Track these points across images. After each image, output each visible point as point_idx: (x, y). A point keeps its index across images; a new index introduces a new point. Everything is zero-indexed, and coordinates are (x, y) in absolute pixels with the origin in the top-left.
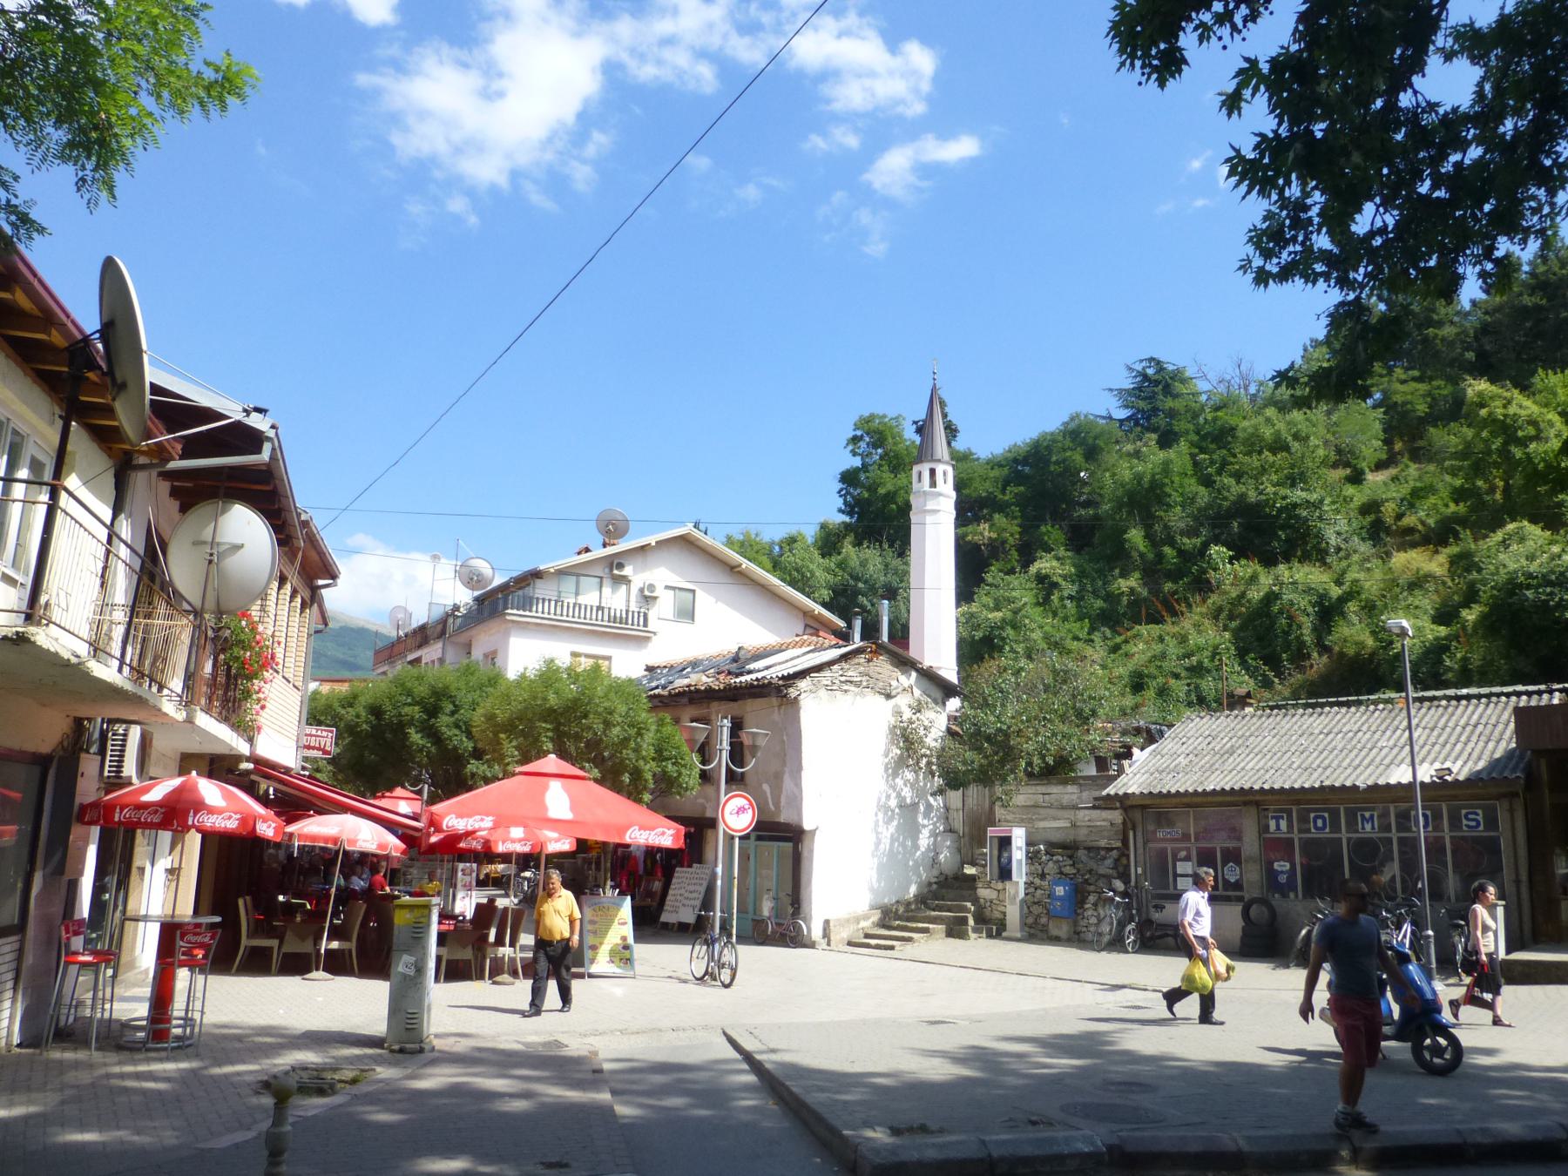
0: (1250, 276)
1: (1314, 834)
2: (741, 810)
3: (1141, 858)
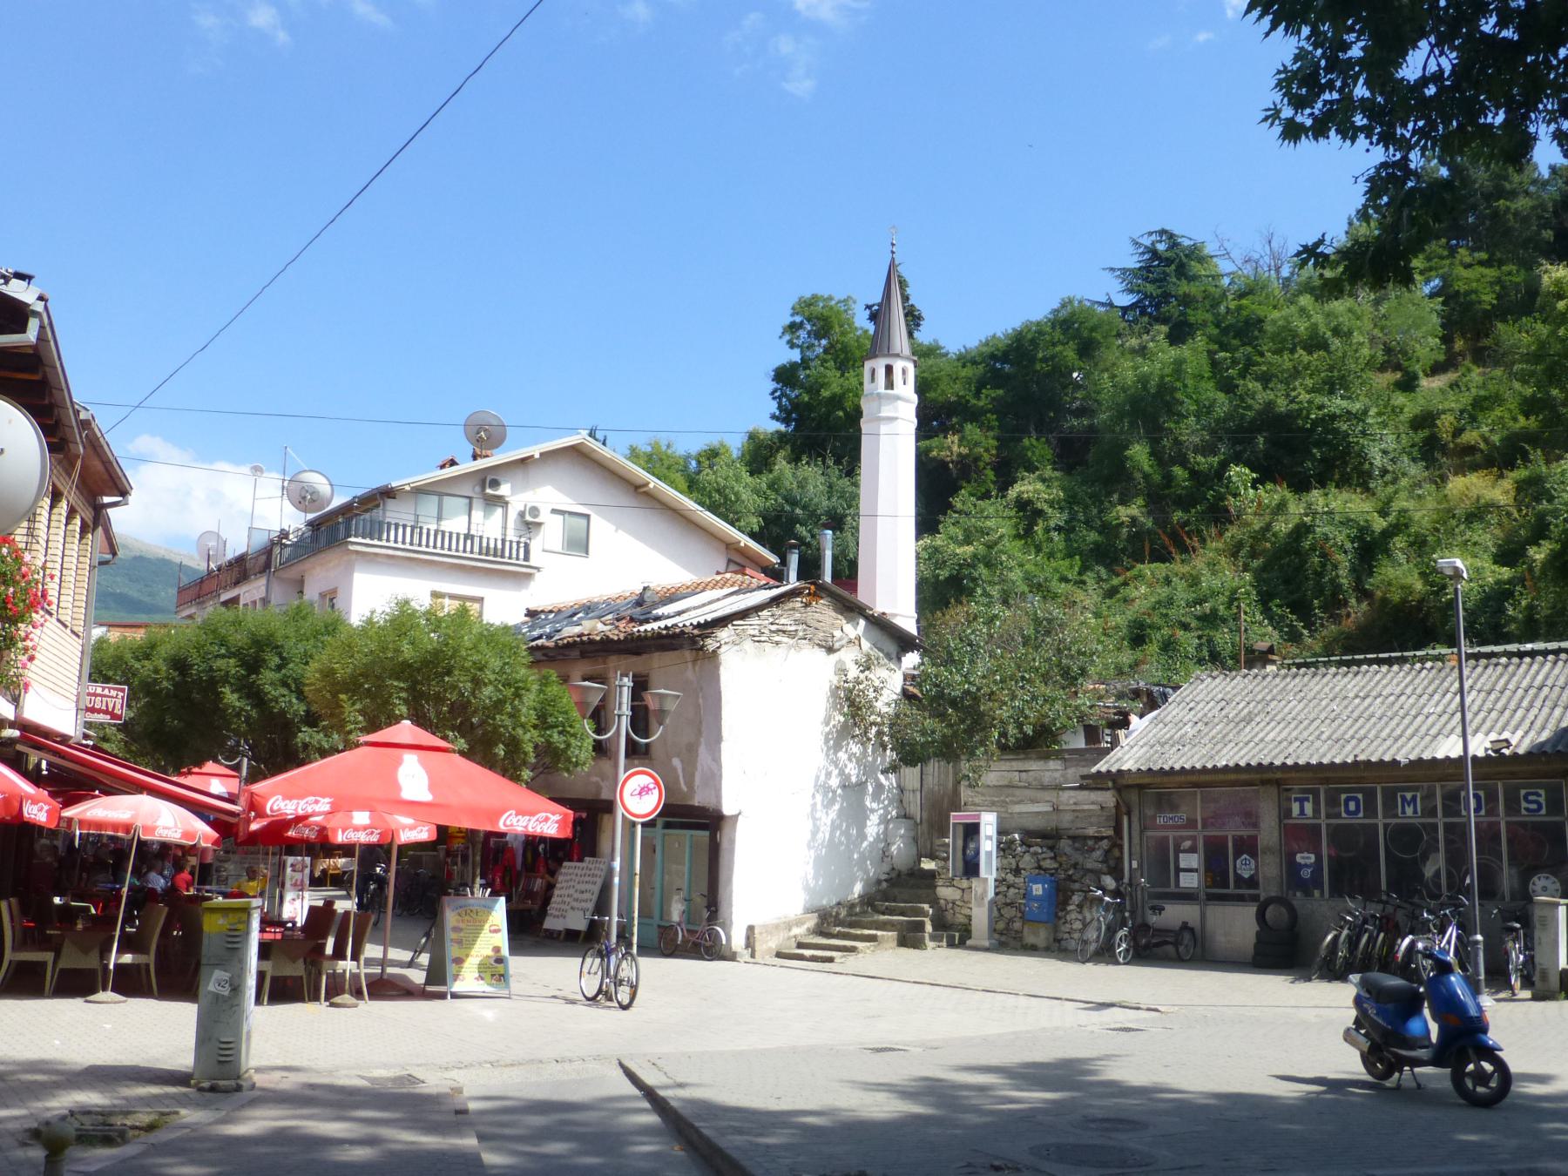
1: (1345, 819)
2: (644, 790)
3: (1136, 849)
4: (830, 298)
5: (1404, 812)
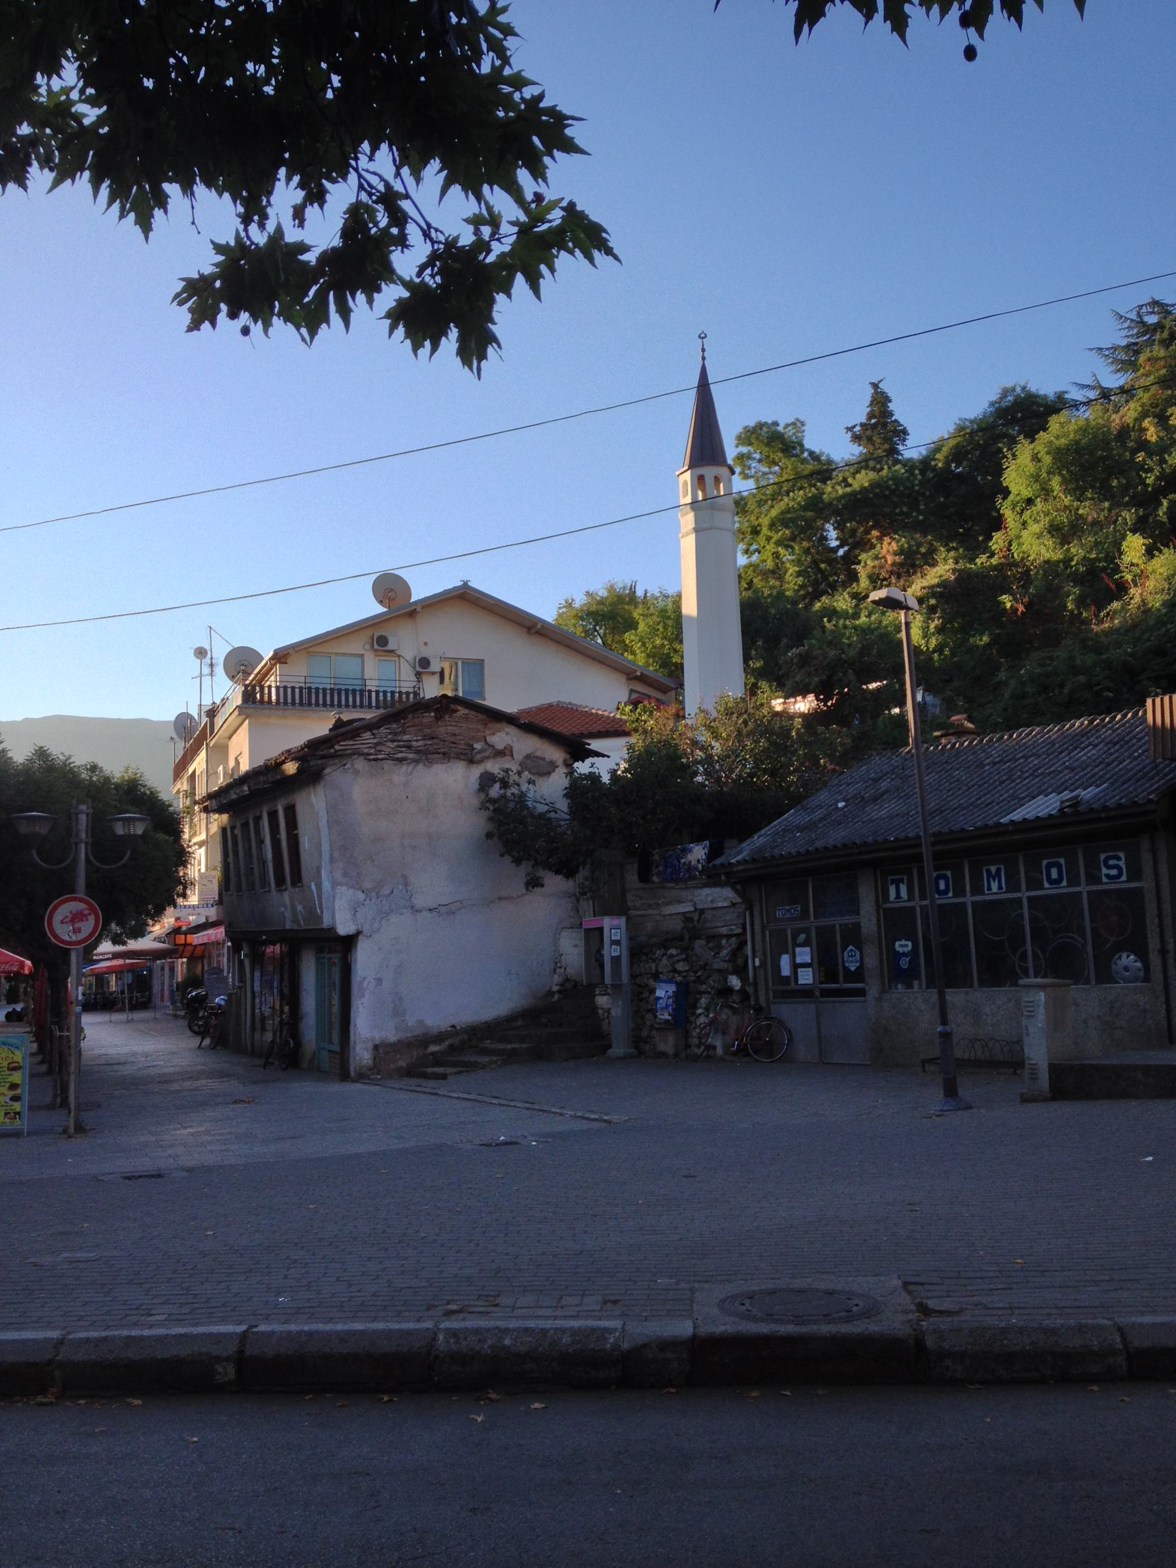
0: (564, 181)
1: (1048, 890)
2: (77, 917)
3: (758, 946)
4: (776, 424)
5: (989, 889)
